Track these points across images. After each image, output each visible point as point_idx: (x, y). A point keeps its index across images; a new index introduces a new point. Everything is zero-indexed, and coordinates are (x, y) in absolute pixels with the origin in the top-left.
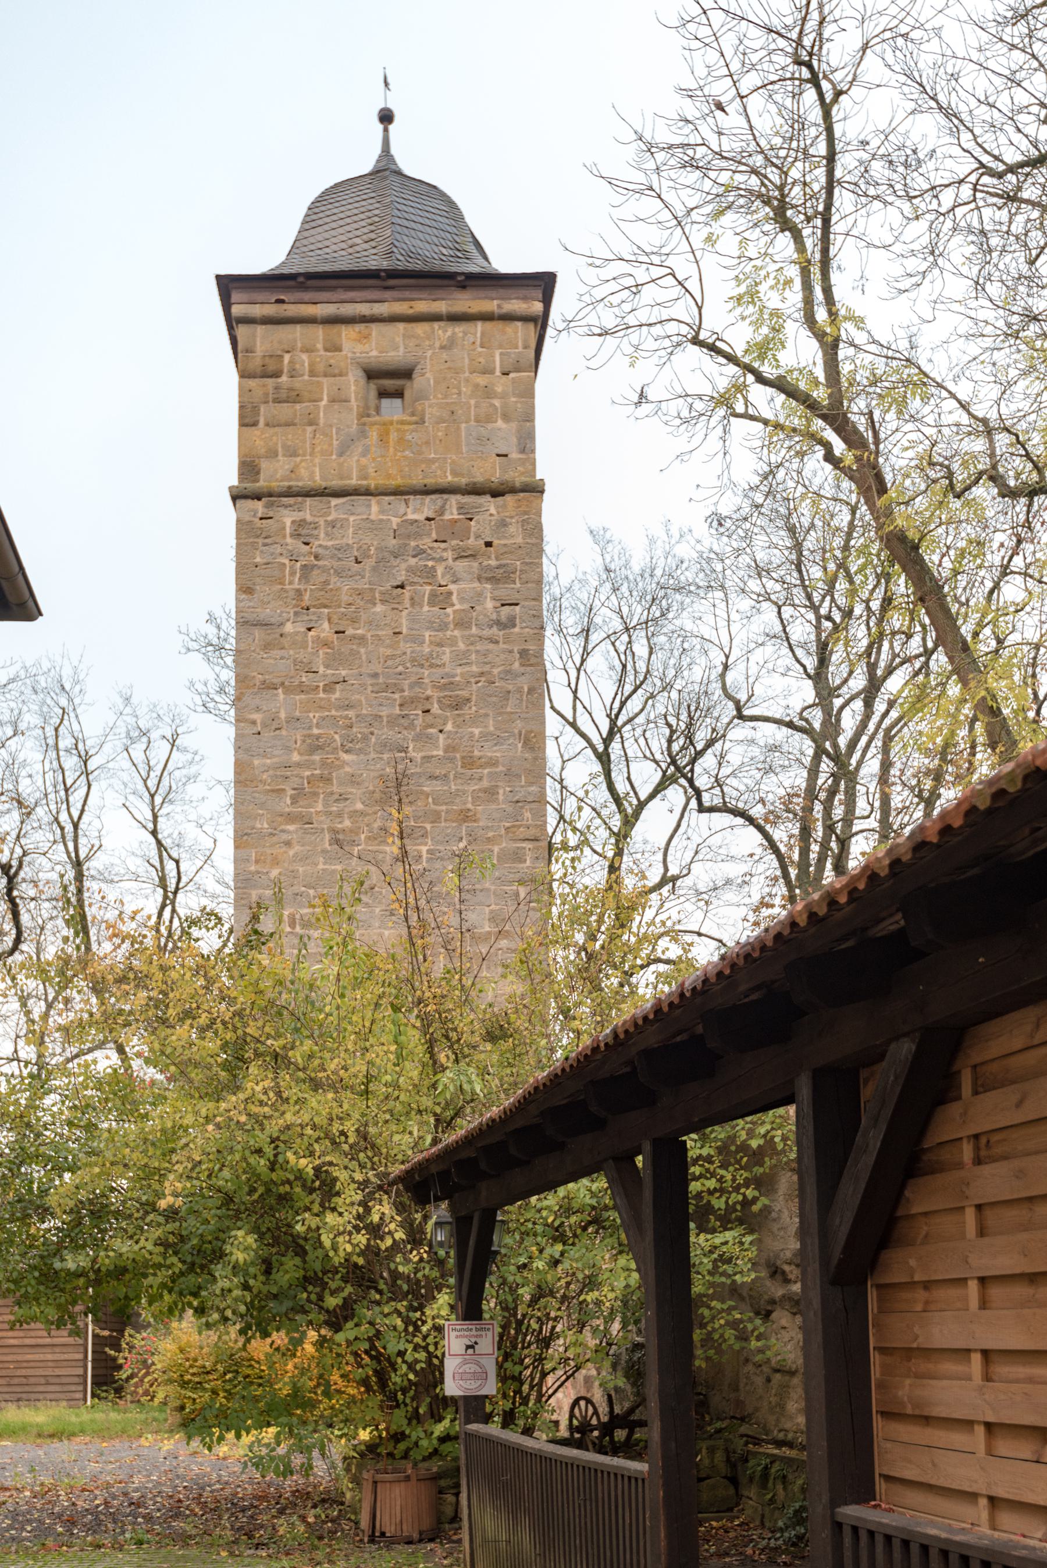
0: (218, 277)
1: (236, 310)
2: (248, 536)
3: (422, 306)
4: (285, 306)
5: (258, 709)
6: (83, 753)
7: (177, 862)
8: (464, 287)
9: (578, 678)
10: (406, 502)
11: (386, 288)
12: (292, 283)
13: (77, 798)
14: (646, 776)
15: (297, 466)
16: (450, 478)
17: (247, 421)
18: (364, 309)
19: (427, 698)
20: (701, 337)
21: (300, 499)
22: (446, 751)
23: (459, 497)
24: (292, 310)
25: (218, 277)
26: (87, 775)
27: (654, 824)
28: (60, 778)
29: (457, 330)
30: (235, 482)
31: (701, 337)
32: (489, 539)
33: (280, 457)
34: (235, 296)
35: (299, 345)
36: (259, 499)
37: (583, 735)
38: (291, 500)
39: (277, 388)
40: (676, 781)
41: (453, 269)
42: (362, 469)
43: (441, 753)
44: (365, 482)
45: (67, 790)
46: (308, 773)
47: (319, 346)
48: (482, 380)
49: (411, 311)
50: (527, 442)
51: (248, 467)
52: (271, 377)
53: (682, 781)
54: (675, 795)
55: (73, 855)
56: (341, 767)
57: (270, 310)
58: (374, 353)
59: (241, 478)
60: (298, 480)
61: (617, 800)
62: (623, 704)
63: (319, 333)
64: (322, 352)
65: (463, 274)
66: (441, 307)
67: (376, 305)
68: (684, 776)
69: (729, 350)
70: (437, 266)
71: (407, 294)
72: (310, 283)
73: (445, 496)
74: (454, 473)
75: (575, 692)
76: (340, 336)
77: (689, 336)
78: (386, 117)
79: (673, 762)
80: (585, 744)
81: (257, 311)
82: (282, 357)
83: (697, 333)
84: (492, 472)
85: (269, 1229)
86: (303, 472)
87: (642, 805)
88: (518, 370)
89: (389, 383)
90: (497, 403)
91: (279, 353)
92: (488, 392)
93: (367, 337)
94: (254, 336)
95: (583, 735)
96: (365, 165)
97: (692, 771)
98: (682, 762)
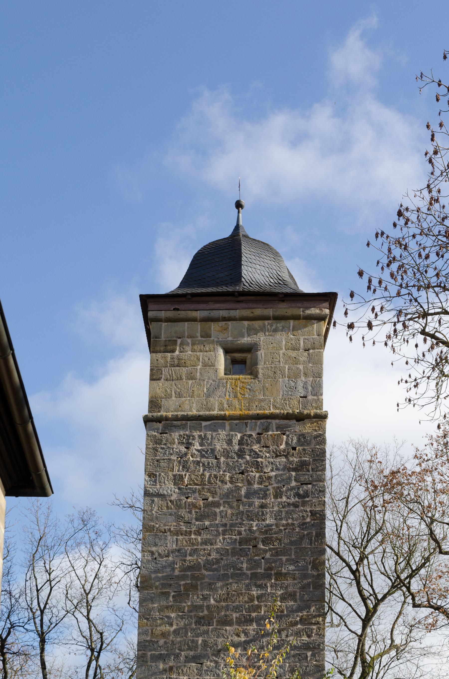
0: (141, 296)
1: (151, 314)
2: (155, 446)
3: (258, 312)
4: (179, 312)
5: (156, 545)
6: (48, 569)
7: (101, 634)
8: (283, 301)
9: (341, 527)
10: (246, 424)
11: (238, 302)
12: (183, 299)
13: (44, 594)
14: (382, 585)
15: (183, 403)
16: (272, 410)
17: (154, 377)
18: (223, 313)
19: (255, 539)
20: (427, 330)
21: (184, 422)
22: (265, 570)
23: (277, 421)
24: (182, 314)
25: (141, 296)
26: (51, 582)
27: (386, 613)
28: (34, 583)
29: (278, 325)
30: (146, 412)
31: (427, 330)
32: (243, 202)
33: (174, 398)
34: (151, 306)
35: (186, 334)
36: (160, 422)
37: (344, 561)
38: (179, 423)
39: (172, 358)
40: (400, 588)
41: (277, 291)
42: (221, 404)
43: (263, 571)
44: (222, 413)
45: (38, 591)
46: (182, 583)
47: (199, 335)
48: (293, 354)
49: (252, 315)
50: (317, 389)
51: (154, 404)
52: (170, 352)
53: (404, 589)
54: (398, 595)
55: (40, 629)
56: (203, 579)
57: (170, 314)
58: (230, 339)
59: (150, 411)
60: (182, 411)
61: (364, 599)
62: (368, 541)
63: (198, 326)
64: (200, 338)
65: (283, 293)
66: (270, 312)
67: (232, 311)
68: (404, 585)
69: (444, 339)
70: (268, 289)
71: (250, 305)
72: (194, 299)
73: (269, 421)
74: (275, 407)
75: (339, 534)
76: (210, 328)
77: (420, 330)
78: (239, 205)
79: (398, 577)
80: (344, 564)
81: (163, 315)
82: (177, 341)
83: (425, 328)
84: (295, 407)
85: (288, 380)
86: (187, 407)
87: (379, 602)
88: (314, 349)
89: (238, 356)
90: (301, 367)
91: (175, 339)
92: (296, 361)
93: (226, 329)
94: (161, 329)
95: (344, 561)
96: (227, 233)
97: (409, 583)
98: (403, 576)
